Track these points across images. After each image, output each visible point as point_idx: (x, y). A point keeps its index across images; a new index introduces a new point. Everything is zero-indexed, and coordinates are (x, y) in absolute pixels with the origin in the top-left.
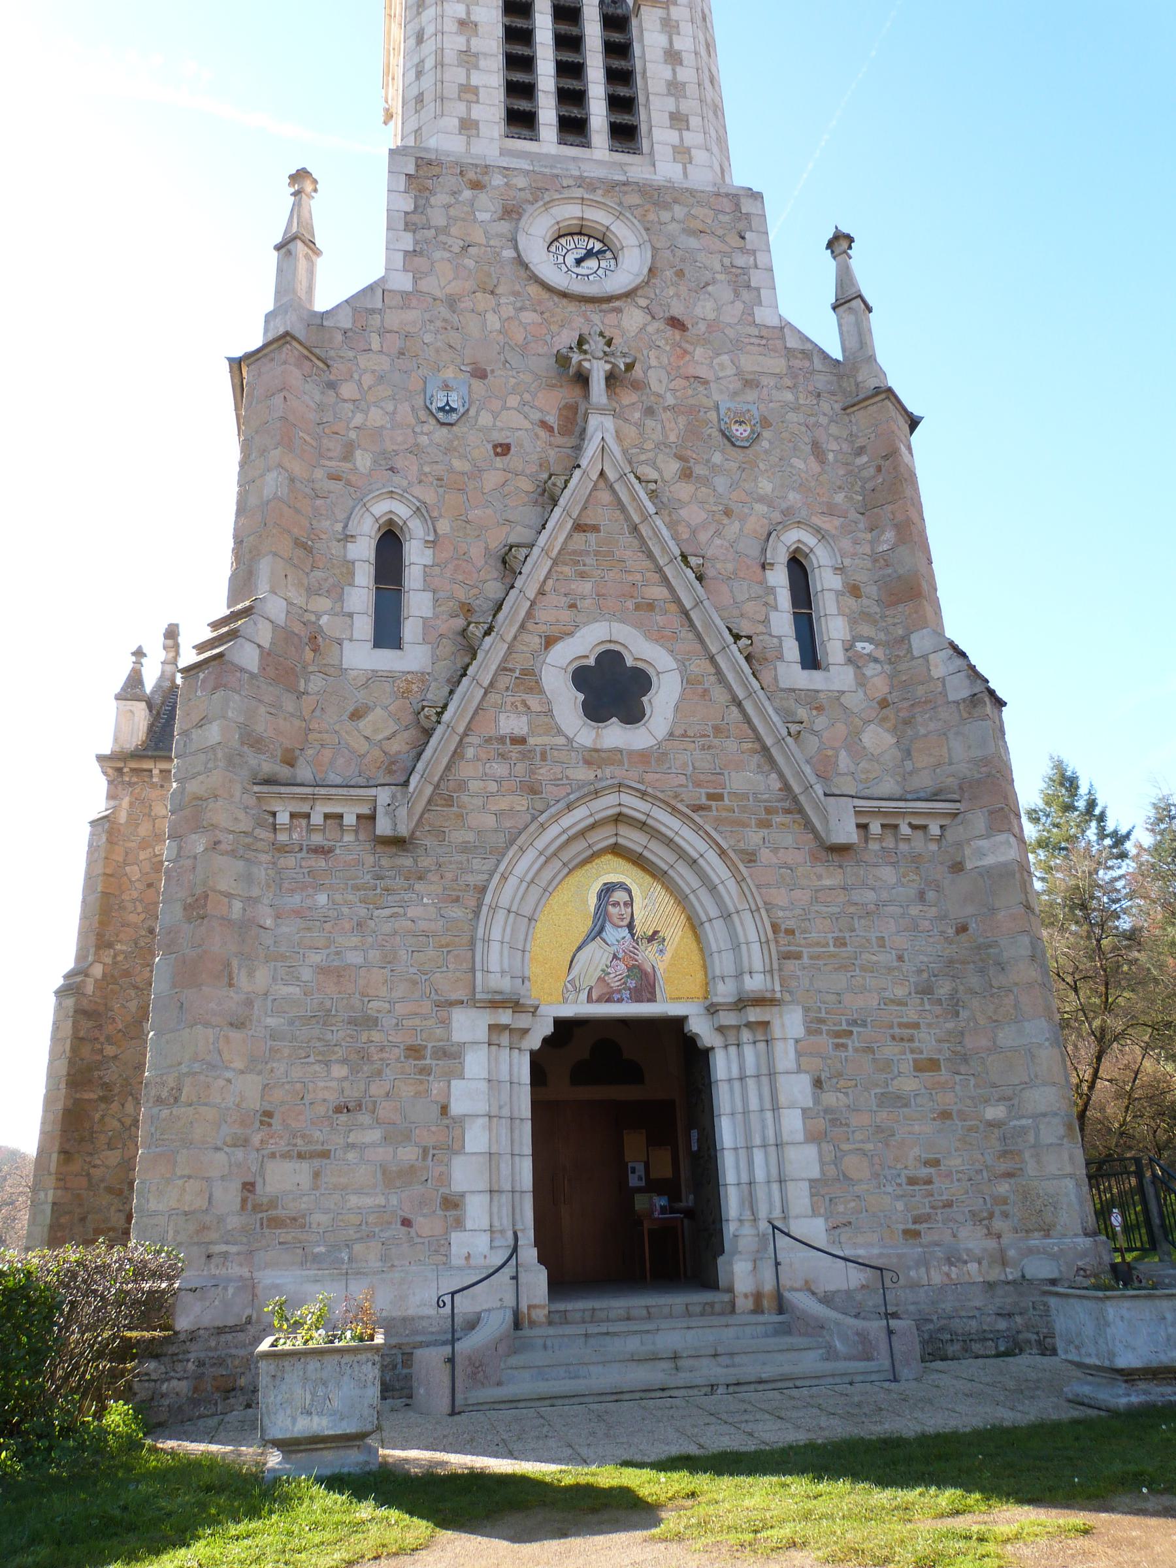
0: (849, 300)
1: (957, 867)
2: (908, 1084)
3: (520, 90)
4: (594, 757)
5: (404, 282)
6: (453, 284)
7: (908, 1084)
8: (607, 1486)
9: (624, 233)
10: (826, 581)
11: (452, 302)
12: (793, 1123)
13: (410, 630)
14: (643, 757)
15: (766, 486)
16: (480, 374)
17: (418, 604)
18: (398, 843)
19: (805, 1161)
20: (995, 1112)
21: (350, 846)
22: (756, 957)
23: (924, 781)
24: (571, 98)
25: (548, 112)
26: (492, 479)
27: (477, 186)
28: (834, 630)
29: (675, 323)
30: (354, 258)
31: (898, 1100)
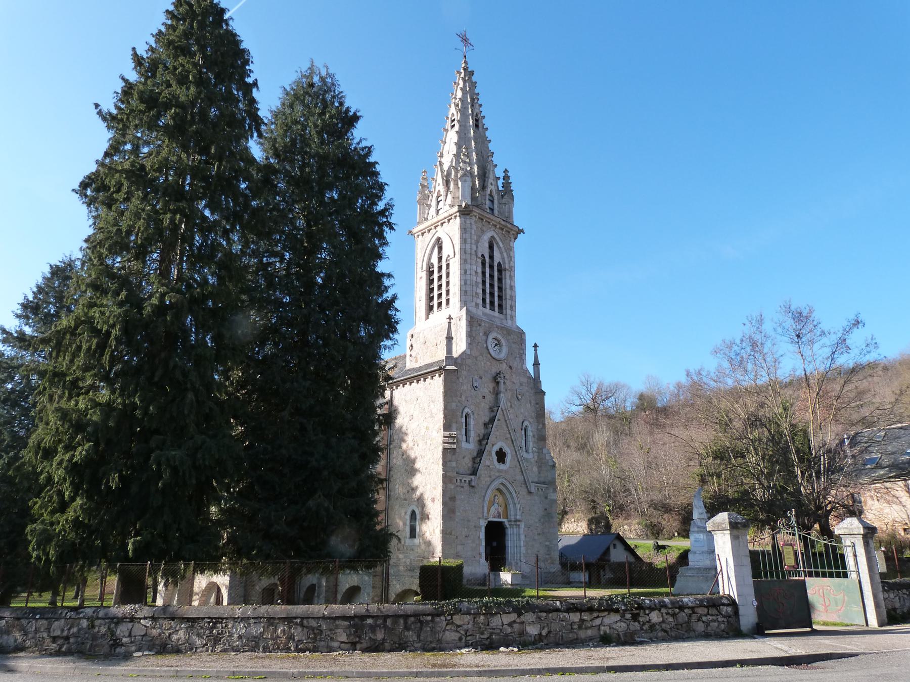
0: (536, 364)
1: (546, 498)
2: (536, 537)
3: (484, 300)
4: (499, 471)
5: (468, 352)
6: (619, 624)
7: (536, 537)
8: (243, 46)
9: (505, 350)
10: (530, 434)
11: (476, 358)
12: (522, 543)
13: (471, 439)
14: (506, 471)
15: (522, 411)
16: (481, 378)
17: (472, 434)
18: (473, 487)
19: (523, 550)
20: (547, 543)
21: (466, 485)
22: (519, 513)
23: (542, 479)
24: (492, 303)
25: (488, 306)
26: (483, 404)
27: (480, 325)
28: (531, 445)
29: (511, 367)
30: (460, 346)
31: (534, 540)
